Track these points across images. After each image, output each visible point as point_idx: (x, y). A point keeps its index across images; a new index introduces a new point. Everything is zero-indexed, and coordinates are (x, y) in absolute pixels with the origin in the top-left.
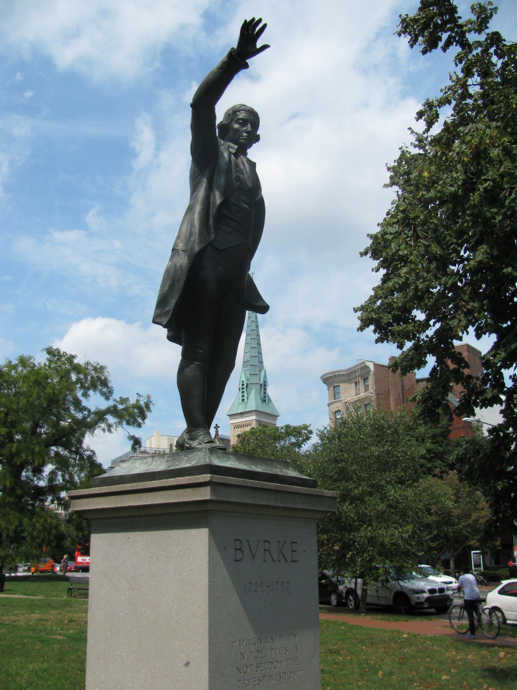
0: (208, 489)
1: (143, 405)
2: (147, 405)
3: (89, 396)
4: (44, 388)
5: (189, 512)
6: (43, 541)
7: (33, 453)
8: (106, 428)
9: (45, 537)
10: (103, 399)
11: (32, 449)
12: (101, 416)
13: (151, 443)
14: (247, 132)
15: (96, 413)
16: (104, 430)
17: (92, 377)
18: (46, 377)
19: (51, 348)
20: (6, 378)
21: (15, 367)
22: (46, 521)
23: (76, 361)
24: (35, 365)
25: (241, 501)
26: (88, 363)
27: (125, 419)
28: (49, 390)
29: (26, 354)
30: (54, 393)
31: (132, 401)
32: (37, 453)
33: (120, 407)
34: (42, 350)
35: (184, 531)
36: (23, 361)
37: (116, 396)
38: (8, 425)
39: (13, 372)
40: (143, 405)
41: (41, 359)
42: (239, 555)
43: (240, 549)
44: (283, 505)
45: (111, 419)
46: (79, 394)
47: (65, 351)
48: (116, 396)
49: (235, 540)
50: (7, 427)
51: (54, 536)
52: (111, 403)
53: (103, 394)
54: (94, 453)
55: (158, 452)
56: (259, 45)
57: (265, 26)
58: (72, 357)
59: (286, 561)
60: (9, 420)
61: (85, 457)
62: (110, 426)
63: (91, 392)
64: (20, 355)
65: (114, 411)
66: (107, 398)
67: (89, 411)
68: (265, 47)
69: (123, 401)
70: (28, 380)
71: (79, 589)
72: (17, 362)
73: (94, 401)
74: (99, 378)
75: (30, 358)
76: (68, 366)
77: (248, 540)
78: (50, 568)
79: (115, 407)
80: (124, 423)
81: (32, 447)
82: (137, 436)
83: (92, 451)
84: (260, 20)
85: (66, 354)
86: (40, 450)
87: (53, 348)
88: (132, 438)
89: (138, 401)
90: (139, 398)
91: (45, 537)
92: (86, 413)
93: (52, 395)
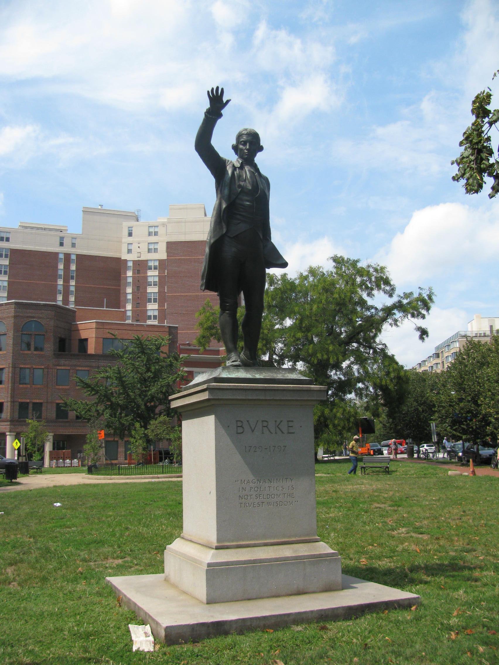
0: (207, 393)
1: (426, 298)
2: (430, 298)
3: (374, 296)
4: (332, 294)
5: (208, 406)
6: (344, 428)
7: (328, 352)
8: (393, 323)
9: (345, 425)
10: (387, 296)
11: (327, 349)
12: (388, 311)
13: (472, 327)
14: (247, 150)
15: (382, 310)
16: (391, 324)
17: (376, 277)
18: (333, 284)
20: (299, 288)
21: (306, 278)
22: (344, 410)
23: (359, 265)
24: (324, 274)
25: (234, 397)
26: (369, 266)
27: (410, 313)
30: (340, 297)
31: (416, 295)
33: (405, 301)
35: (202, 418)
36: (312, 271)
37: (399, 292)
40: (426, 298)
41: (329, 267)
42: (240, 430)
43: (241, 426)
44: (272, 398)
45: (398, 315)
46: (365, 296)
47: (349, 257)
48: (399, 292)
49: (237, 421)
50: (303, 332)
51: (353, 423)
52: (395, 299)
53: (385, 292)
54: (386, 346)
55: (478, 335)
56: (224, 101)
57: (222, 90)
58: (355, 262)
59: (283, 433)
60: (304, 325)
61: (378, 350)
62: (396, 321)
63: (375, 292)
65: (399, 306)
66: (391, 296)
67: (376, 309)
68: (228, 101)
69: (407, 295)
71: (371, 467)
73: (379, 300)
74: (382, 278)
75: (319, 268)
76: (351, 271)
77: (248, 421)
78: (367, 451)
79: (400, 302)
80: (409, 316)
81: (327, 346)
82: (423, 327)
83: (383, 344)
84: (218, 88)
85: (350, 260)
86: (334, 349)
88: (419, 329)
89: (420, 294)
90: (421, 291)
91: (345, 425)
92: (373, 311)
93: (339, 299)
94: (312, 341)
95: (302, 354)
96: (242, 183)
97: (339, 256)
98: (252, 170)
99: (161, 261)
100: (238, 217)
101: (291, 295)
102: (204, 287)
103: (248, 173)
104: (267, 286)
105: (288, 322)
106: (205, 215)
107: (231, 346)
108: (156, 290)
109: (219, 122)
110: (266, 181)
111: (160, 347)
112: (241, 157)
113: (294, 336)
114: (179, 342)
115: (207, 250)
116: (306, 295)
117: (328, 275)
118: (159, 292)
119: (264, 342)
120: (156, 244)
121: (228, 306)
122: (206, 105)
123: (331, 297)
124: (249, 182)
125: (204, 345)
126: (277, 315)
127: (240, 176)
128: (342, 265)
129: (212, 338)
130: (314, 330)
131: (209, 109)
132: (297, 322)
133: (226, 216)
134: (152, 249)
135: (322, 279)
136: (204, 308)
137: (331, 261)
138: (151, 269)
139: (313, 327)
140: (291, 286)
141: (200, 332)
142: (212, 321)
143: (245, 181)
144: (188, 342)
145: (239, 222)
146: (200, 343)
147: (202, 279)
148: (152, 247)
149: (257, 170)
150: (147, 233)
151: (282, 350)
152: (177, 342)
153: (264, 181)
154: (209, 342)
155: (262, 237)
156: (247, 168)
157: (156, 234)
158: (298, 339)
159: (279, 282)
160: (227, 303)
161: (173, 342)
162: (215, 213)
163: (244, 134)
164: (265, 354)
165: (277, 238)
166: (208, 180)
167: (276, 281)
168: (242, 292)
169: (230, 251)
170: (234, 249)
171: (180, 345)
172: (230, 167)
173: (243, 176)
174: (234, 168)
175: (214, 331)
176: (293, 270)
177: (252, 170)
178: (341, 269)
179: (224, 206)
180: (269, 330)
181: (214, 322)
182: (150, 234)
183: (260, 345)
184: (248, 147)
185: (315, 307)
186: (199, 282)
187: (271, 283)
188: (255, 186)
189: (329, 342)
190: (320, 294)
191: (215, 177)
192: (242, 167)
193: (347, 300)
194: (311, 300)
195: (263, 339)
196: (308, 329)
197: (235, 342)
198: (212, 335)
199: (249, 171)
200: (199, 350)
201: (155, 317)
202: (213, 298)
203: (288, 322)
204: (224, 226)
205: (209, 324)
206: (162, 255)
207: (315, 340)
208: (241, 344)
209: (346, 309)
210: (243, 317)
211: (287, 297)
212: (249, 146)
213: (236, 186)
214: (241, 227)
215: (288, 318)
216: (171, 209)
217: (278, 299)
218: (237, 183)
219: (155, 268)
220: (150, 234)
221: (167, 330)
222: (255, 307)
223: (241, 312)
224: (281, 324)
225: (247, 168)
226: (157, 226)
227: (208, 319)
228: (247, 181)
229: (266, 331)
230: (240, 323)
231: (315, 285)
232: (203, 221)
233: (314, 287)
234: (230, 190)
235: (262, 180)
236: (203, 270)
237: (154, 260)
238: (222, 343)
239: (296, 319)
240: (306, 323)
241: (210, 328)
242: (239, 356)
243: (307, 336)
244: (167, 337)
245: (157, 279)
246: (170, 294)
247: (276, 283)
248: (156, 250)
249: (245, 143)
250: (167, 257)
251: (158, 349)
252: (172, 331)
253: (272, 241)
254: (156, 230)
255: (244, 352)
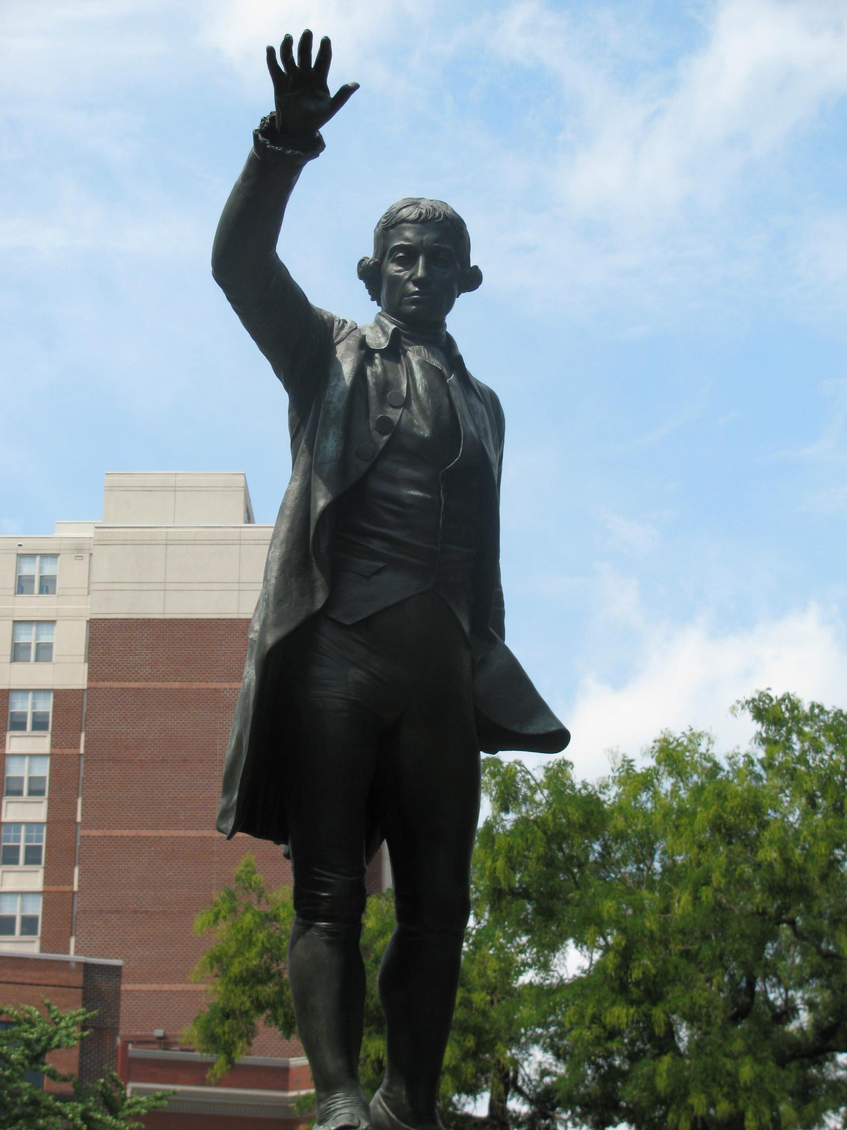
4: (752, 845)
7: (734, 1090)
11: (729, 1074)
18: (754, 807)
19: (764, 696)
20: (619, 822)
21: (647, 781)
24: (716, 767)
28: (768, 854)
29: (678, 730)
30: (787, 862)
32: (747, 1089)
34: (733, 709)
38: (636, 993)
39: (644, 797)
41: (735, 739)
47: (818, 701)
50: (632, 1003)
57: (326, 44)
60: (636, 974)
64: (659, 736)
68: (346, 92)
70: (691, 824)
72: (651, 763)
75: (695, 738)
81: (729, 1064)
84: (307, 37)
85: (822, 710)
86: (759, 1079)
87: (772, 694)
93: (779, 869)
94: (665, 1043)
95: (629, 1094)
96: (395, 415)
97: (777, 693)
98: (436, 363)
99: (62, 697)
100: (376, 545)
101: (587, 850)
102: (230, 824)
103: (418, 375)
104: (486, 809)
105: (573, 961)
106: (249, 518)
107: (333, 1063)
108: (36, 811)
109: (311, 170)
110: (491, 404)
111: (45, 1051)
112: (392, 309)
113: (596, 1019)
114: (127, 1028)
115: (250, 673)
116: (644, 848)
117: (737, 772)
118: (52, 822)
119: (470, 1042)
120: (44, 628)
121: (327, 900)
122: (262, 99)
123: (746, 860)
124: (422, 410)
125: (228, 1050)
126: (527, 932)
127: (386, 386)
128: (789, 732)
129: (260, 1021)
130: (675, 993)
131: (272, 118)
132: (612, 960)
133: (323, 543)
134: (28, 646)
135: (709, 787)
136: (232, 896)
137: (748, 715)
138: (21, 726)
139: (672, 982)
140: (588, 814)
141: (207, 990)
142: (265, 950)
143: (406, 404)
144: (159, 1033)
145: (380, 565)
146: (212, 1040)
147: (227, 789)
148: (27, 636)
149: (456, 363)
150: (12, 583)
151: (544, 1073)
152: (115, 1030)
153: (480, 408)
154: (249, 1034)
155: (466, 627)
156: (415, 355)
157: (47, 585)
158: (613, 1034)
159: (538, 797)
160: (326, 887)
161: (99, 1031)
162: (285, 527)
163: (404, 221)
164: (472, 1090)
165: (526, 637)
166: (262, 396)
167: (524, 790)
168: (385, 846)
169: (339, 680)
170: (355, 674)
171: (125, 1044)
172: (348, 348)
173: (399, 385)
174: (366, 353)
175: (268, 991)
176: (590, 761)
177: (436, 363)
178: (787, 747)
179: (321, 503)
180: (491, 989)
181: (270, 952)
182: (22, 586)
183: (450, 1055)
184: (420, 273)
185: (682, 903)
186: (214, 796)
187: (505, 802)
188: (447, 427)
189: (738, 1045)
190: (701, 847)
191: (288, 386)
192: (394, 351)
193: (814, 873)
194: (666, 870)
195: (465, 1029)
196: (653, 992)
197: (349, 1046)
198: (260, 1007)
199: (423, 365)
200: (206, 1066)
201: (29, 925)
202: (269, 869)
203: (573, 961)
204: (320, 581)
205: (253, 959)
206: (71, 671)
207: (684, 1034)
208: (375, 1046)
209: (809, 909)
210: (390, 937)
211: (570, 858)
212: (426, 267)
213: (372, 424)
214: (385, 588)
215: (570, 942)
216: (110, 489)
217: (532, 865)
218: (375, 414)
219: (39, 724)
220: (22, 586)
221: (78, 979)
222: (433, 911)
223: (379, 915)
224: (545, 967)
225: (415, 355)
226: (55, 556)
227: (248, 940)
228: (414, 407)
229: (479, 998)
230: (377, 961)
231: (681, 812)
232: (240, 542)
233: (678, 818)
234: (347, 437)
235: (474, 400)
236: (229, 753)
237: (32, 756)
238: (296, 1041)
239: (607, 949)
240: (645, 964)
241: (253, 978)
242: (366, 1107)
243: (648, 1016)
244: (78, 1012)
245: (43, 769)
246: (94, 833)
247: (525, 799)
248: (44, 652)
249: (408, 257)
250: (90, 679)
251: (37, 1058)
252: (98, 987)
253: (507, 643)
254: (44, 639)
255: (388, 1089)
